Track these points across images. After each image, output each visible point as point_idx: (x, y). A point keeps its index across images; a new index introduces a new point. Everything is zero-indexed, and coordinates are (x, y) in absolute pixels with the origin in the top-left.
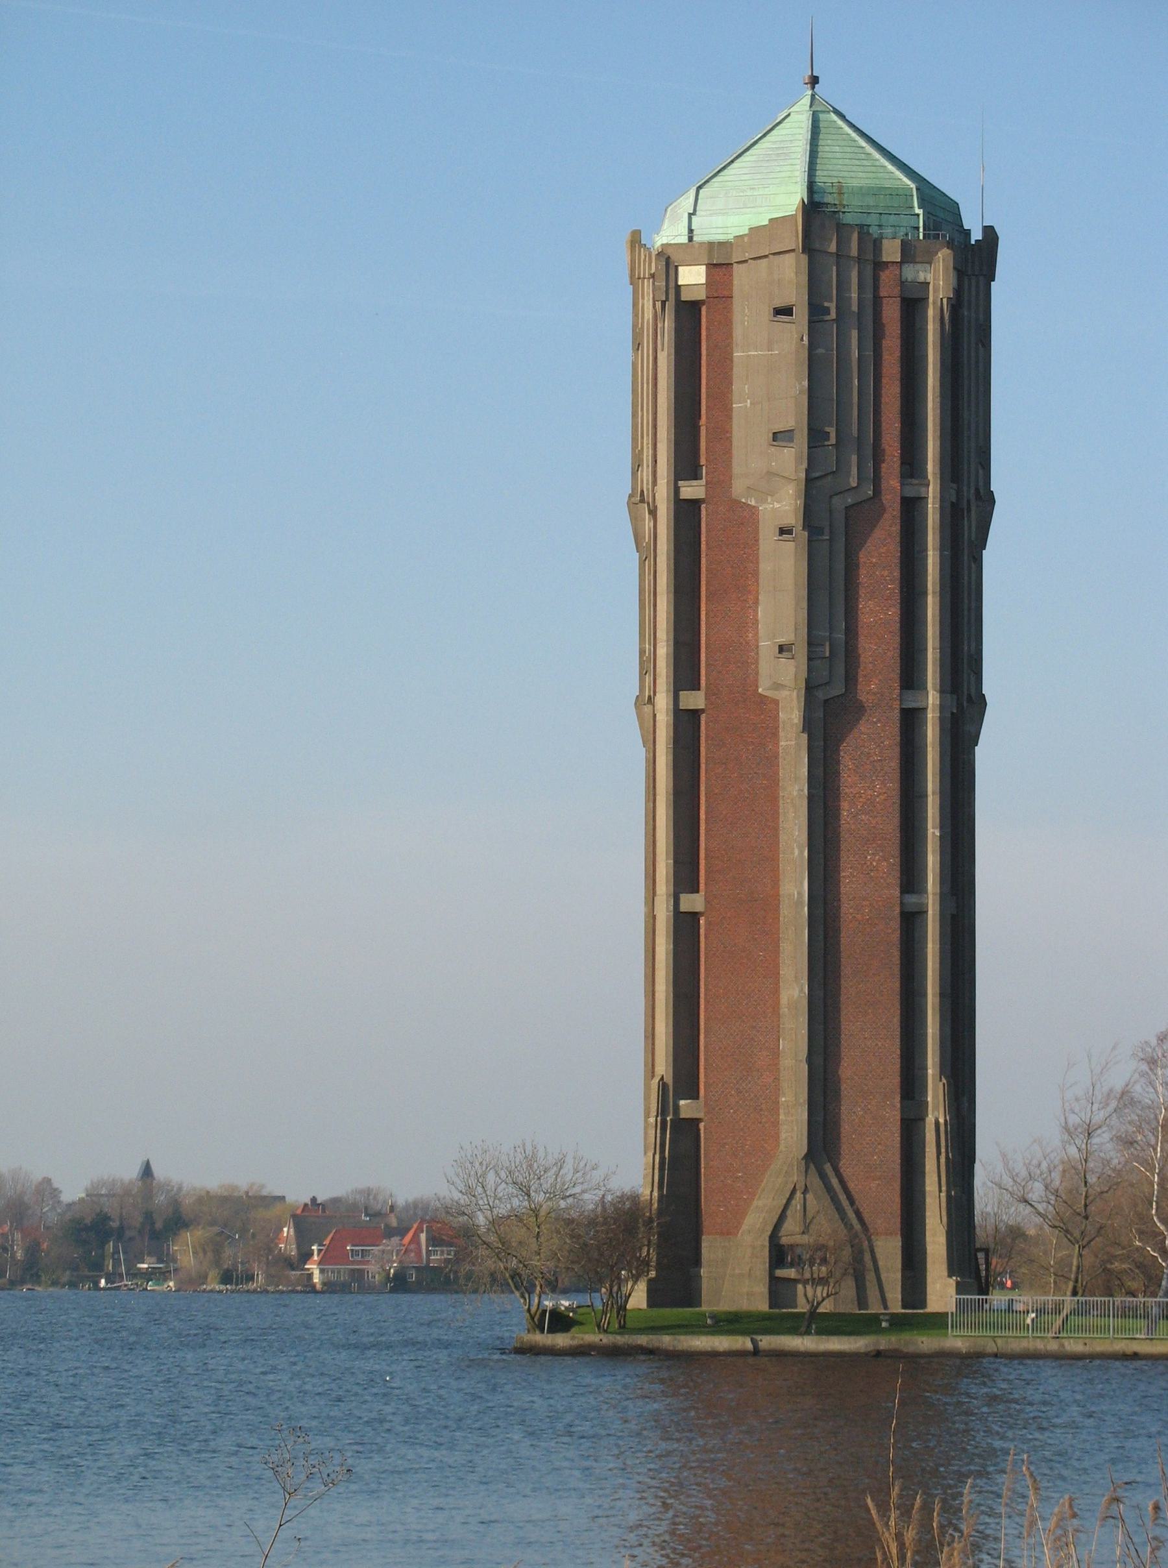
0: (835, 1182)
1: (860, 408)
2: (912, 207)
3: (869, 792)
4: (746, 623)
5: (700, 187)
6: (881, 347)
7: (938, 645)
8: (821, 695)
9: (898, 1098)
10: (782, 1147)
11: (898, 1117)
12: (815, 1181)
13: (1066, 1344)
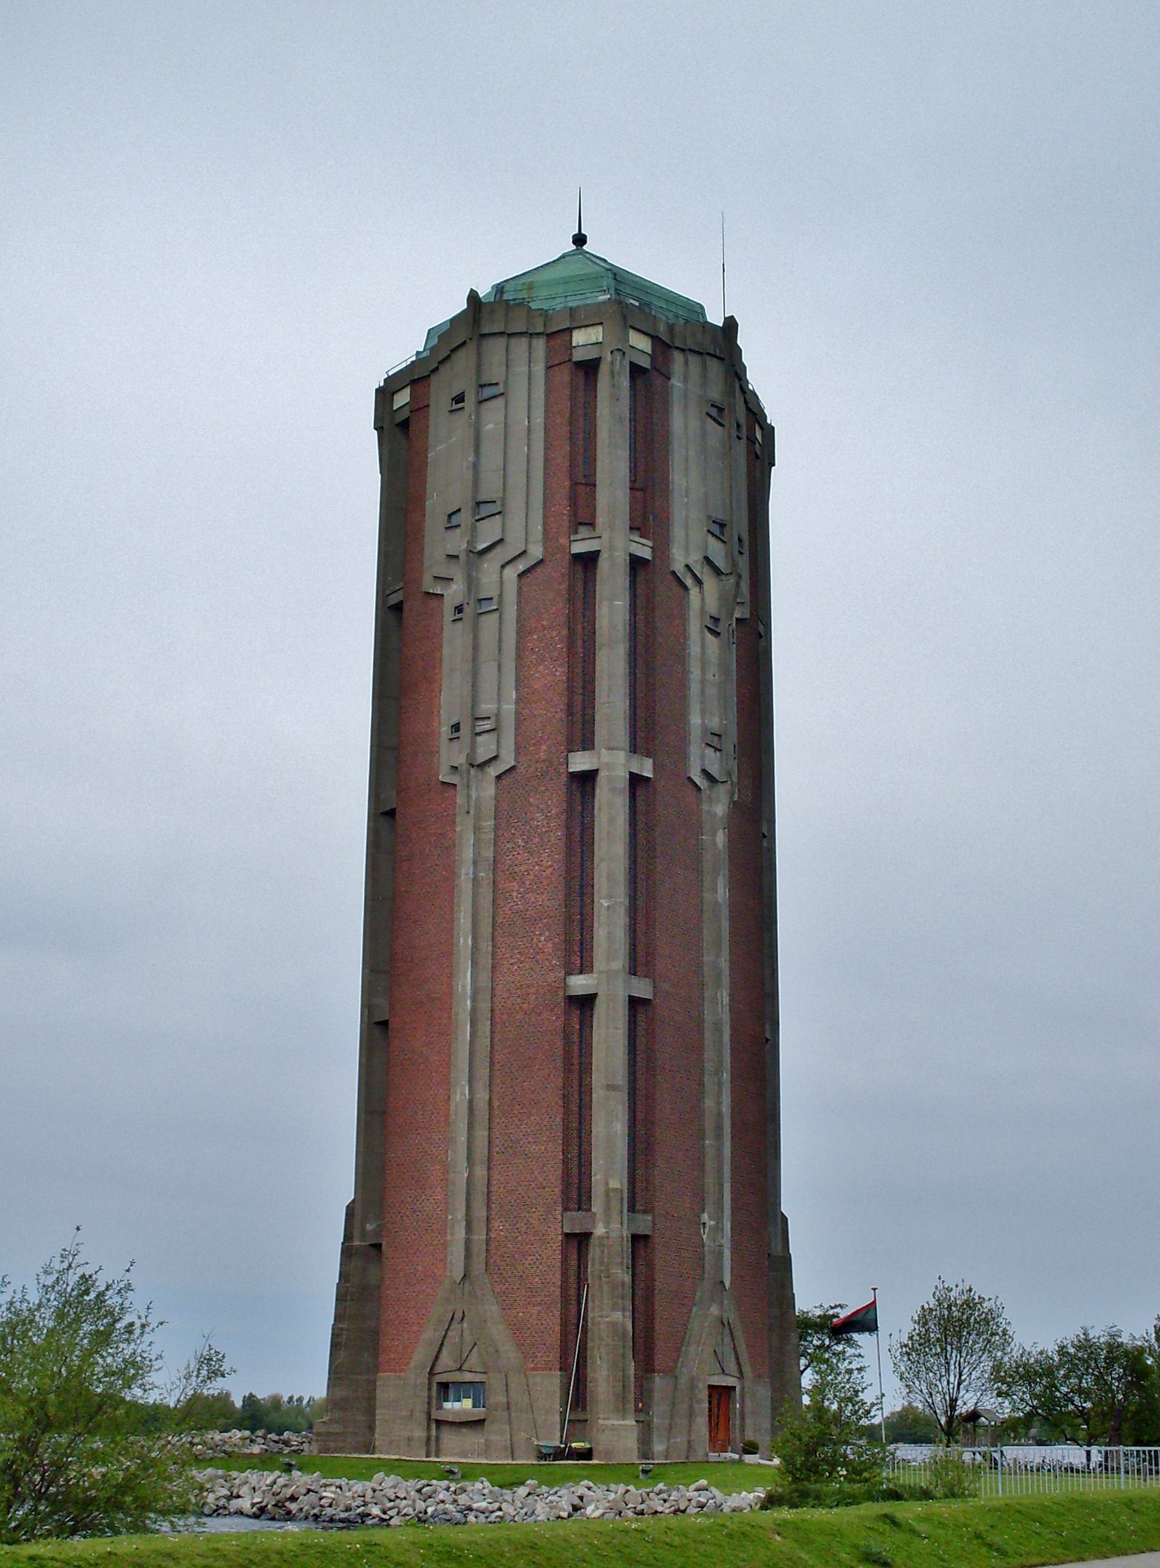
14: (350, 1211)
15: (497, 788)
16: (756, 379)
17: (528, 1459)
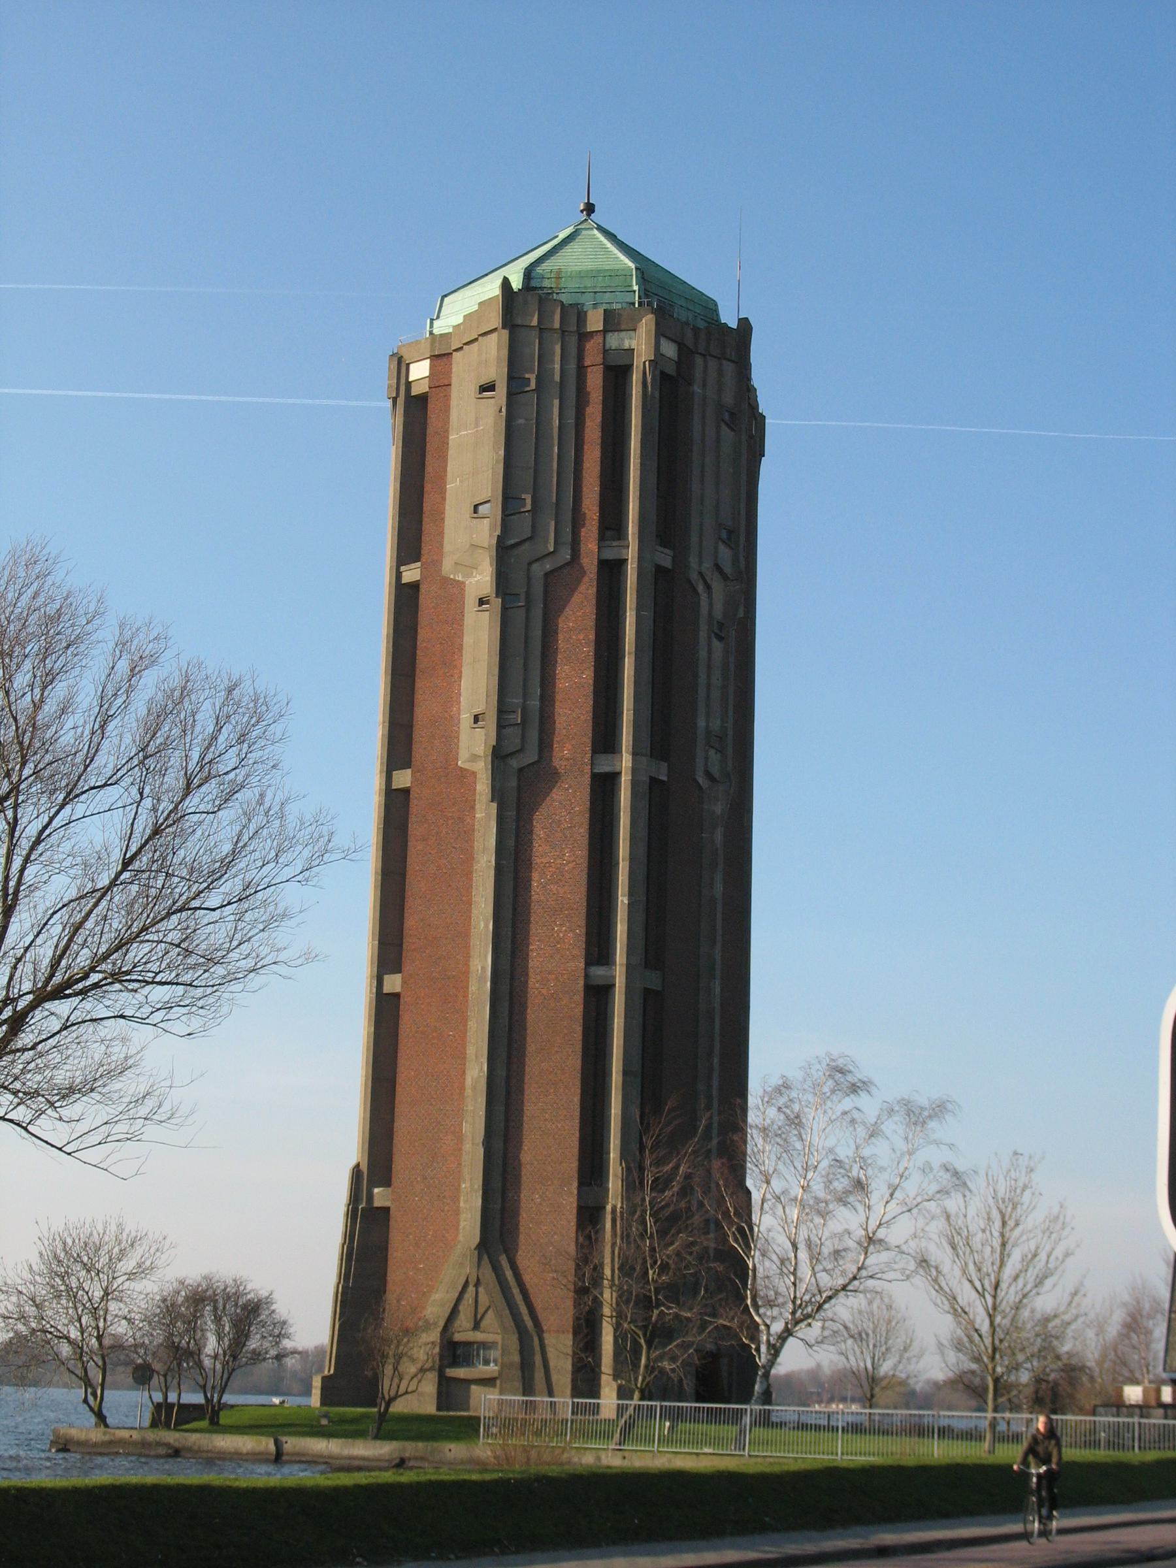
0: (509, 1274)
1: (621, 512)
2: (631, 286)
3: (559, 861)
4: (450, 698)
5: (446, 296)
6: (584, 415)
7: (632, 707)
8: (514, 763)
9: (575, 1184)
10: (461, 1238)
11: (575, 1205)
12: (488, 1273)
13: (603, 1457)
14: (356, 1172)
15: (519, 779)
16: (758, 378)
17: (515, 1395)
